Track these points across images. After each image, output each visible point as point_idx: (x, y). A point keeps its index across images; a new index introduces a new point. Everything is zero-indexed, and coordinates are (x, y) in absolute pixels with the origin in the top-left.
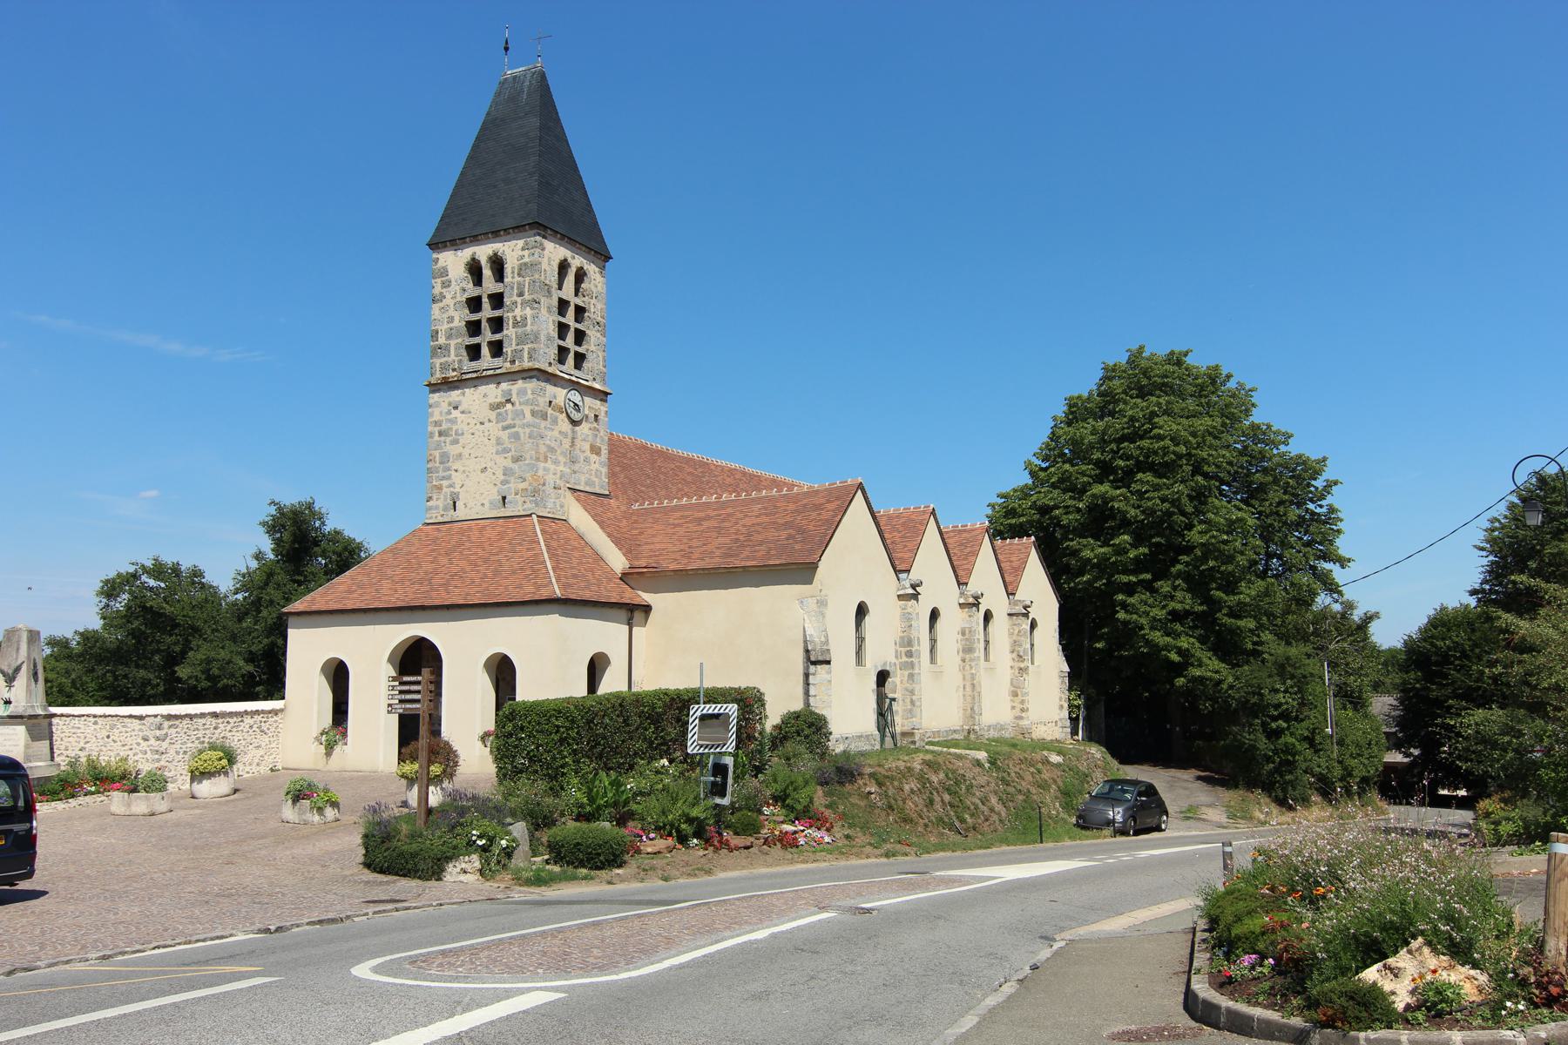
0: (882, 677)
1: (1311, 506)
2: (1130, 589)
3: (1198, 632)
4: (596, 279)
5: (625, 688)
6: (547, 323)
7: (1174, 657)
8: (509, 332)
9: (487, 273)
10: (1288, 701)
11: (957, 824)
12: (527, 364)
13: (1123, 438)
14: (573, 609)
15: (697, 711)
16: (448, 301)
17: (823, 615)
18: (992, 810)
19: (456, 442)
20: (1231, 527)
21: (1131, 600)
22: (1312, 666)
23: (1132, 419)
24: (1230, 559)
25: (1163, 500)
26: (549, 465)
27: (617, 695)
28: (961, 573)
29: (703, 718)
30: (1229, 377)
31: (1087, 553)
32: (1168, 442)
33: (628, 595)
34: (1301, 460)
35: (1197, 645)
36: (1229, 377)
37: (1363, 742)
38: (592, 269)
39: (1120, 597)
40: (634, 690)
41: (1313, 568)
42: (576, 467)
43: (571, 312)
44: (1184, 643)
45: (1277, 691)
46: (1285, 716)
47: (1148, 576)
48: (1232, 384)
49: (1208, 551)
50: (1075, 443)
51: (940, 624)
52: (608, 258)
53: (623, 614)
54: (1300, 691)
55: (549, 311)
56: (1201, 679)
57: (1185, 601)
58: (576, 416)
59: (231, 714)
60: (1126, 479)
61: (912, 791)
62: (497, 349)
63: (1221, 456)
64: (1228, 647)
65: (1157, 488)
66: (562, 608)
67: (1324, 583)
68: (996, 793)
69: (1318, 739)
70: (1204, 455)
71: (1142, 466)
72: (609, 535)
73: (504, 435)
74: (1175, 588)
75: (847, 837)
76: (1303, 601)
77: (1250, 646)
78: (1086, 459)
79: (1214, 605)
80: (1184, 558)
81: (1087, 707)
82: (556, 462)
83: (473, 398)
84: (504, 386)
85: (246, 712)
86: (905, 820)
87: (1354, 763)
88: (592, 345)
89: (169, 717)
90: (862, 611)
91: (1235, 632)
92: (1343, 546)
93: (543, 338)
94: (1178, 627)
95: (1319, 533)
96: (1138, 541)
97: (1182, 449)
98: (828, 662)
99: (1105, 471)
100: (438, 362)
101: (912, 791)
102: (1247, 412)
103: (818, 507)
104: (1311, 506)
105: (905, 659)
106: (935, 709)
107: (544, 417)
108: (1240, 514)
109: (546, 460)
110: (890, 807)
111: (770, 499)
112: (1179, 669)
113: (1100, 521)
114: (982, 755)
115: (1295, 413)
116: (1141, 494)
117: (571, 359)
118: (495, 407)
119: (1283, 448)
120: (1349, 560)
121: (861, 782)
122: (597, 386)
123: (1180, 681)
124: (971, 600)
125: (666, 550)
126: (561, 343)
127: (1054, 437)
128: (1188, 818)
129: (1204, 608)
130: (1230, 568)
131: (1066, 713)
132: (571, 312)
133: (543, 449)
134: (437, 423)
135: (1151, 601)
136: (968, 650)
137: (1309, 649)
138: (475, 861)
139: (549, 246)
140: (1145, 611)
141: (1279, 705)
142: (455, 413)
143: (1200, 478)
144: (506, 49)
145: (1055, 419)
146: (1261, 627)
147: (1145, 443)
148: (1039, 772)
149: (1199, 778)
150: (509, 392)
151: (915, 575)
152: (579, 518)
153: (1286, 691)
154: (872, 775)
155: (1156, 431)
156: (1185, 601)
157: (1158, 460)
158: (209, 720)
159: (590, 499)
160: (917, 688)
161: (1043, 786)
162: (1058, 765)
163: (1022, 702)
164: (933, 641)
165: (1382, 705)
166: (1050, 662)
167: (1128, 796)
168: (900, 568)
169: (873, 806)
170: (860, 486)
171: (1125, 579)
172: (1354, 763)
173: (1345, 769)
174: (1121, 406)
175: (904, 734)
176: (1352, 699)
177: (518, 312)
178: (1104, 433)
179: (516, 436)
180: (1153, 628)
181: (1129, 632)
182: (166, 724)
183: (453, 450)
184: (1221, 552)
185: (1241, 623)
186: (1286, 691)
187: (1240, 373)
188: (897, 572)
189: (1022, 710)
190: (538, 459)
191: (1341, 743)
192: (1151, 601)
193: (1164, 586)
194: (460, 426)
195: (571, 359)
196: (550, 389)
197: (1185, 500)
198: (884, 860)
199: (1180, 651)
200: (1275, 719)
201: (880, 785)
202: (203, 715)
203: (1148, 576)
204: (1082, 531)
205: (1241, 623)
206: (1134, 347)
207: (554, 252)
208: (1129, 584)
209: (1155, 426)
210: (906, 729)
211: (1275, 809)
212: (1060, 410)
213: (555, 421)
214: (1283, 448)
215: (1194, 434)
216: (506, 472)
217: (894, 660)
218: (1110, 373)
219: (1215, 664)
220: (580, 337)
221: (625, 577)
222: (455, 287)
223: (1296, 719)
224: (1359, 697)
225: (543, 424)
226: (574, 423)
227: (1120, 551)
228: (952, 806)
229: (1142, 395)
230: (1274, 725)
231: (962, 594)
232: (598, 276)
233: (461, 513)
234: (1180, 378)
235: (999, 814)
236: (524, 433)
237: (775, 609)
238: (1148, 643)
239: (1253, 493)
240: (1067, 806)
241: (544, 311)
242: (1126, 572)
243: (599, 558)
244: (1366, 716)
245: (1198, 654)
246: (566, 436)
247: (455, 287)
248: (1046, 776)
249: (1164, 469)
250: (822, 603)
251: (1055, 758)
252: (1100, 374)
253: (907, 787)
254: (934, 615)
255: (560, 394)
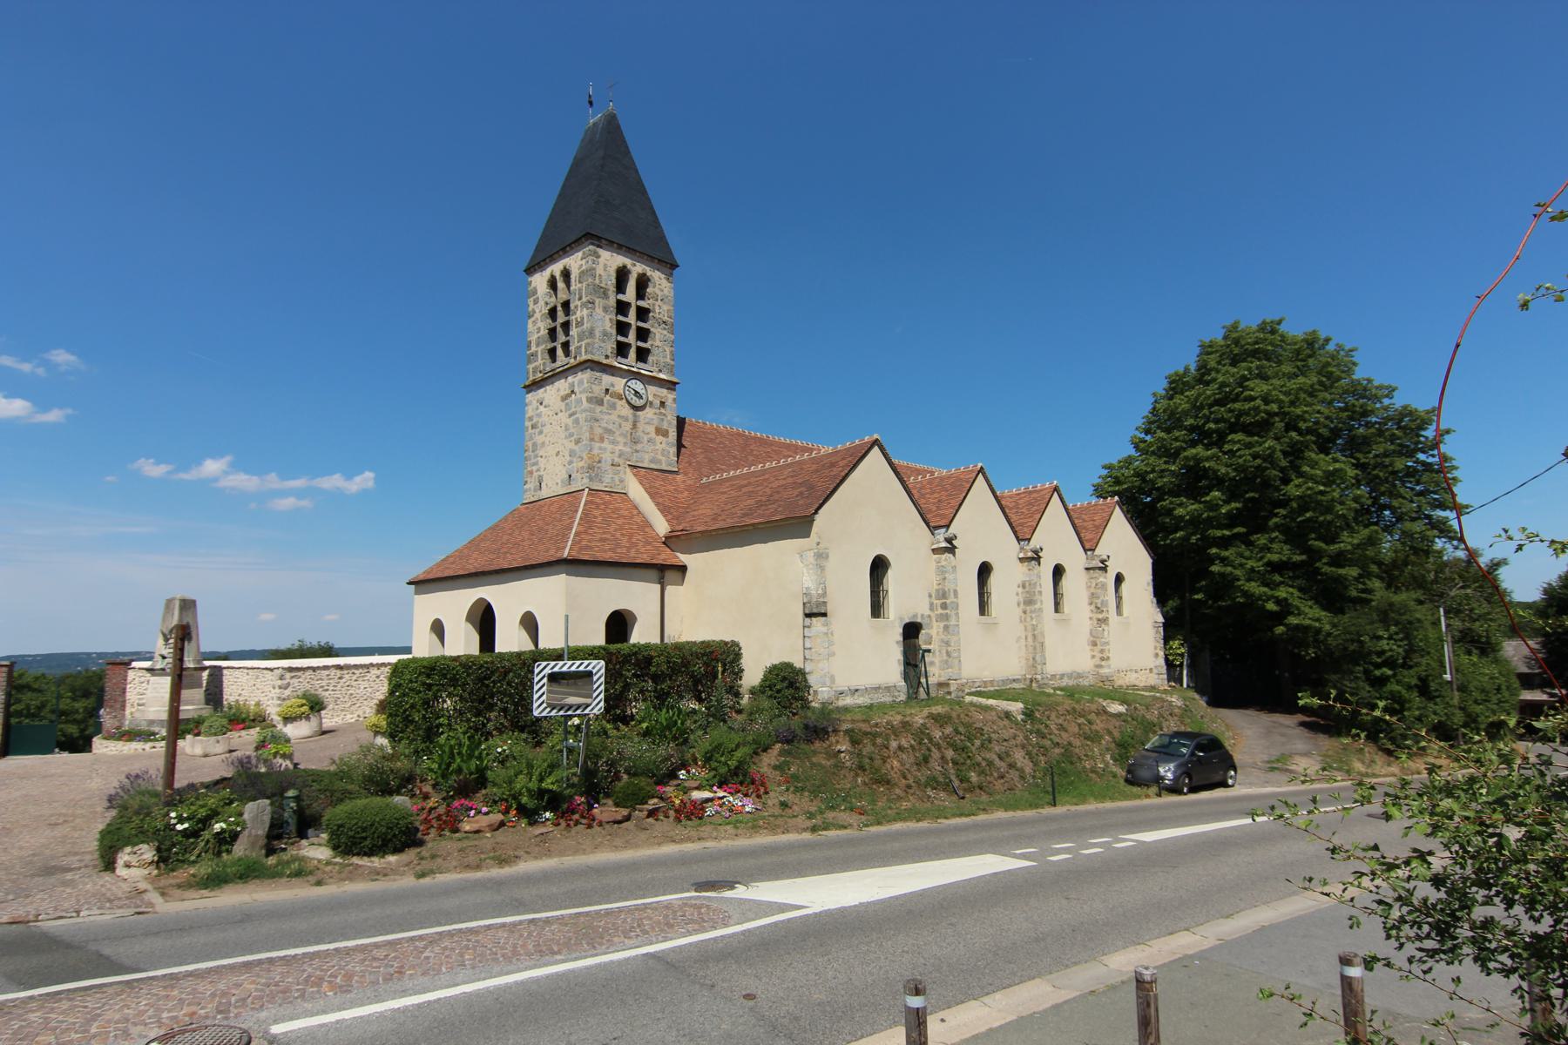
0: (911, 631)
1: (1421, 456)
2: (1224, 543)
3: (1298, 582)
4: (660, 283)
5: (658, 641)
6: (605, 322)
7: (1271, 606)
8: (574, 332)
9: (561, 285)
10: (1395, 649)
11: (956, 783)
12: (584, 357)
13: (1218, 403)
14: (582, 568)
15: (543, 669)
16: (538, 315)
17: (822, 568)
18: (1012, 766)
19: (541, 433)
20: (1331, 478)
21: (1225, 554)
22: (1421, 613)
23: (1223, 385)
24: (1329, 509)
25: (1255, 456)
26: (606, 444)
27: (647, 646)
28: (1086, 535)
29: (554, 678)
30: (1327, 340)
31: (1180, 511)
32: (1258, 401)
33: (665, 557)
34: (1407, 412)
35: (1296, 593)
36: (1327, 340)
37: (1488, 687)
38: (656, 276)
39: (1214, 551)
40: (571, 644)
41: (1428, 517)
42: (639, 447)
43: (633, 312)
44: (1282, 593)
45: (1380, 638)
46: (1389, 663)
47: (1241, 530)
48: (1331, 347)
49: (1305, 503)
50: (1172, 414)
51: (1124, 586)
52: (674, 266)
53: (654, 574)
54: (1407, 637)
55: (605, 309)
56: (1297, 627)
57: (1281, 552)
58: (639, 403)
59: (356, 667)
60: (1220, 440)
61: (900, 748)
62: (642, 355)
63: (1317, 412)
64: (1332, 597)
65: (1249, 446)
66: (570, 568)
67: (1441, 531)
68: (1023, 747)
69: (1433, 686)
70: (1298, 411)
71: (1234, 428)
72: (657, 504)
73: (570, 421)
74: (1272, 540)
75: (784, 805)
76: (1422, 550)
77: (1354, 593)
78: (1180, 427)
79: (1315, 555)
80: (1283, 512)
81: (1192, 656)
82: (613, 442)
83: (552, 393)
84: (570, 379)
85: (372, 665)
86: (878, 782)
87: (1478, 709)
88: (659, 339)
89: (291, 669)
90: (879, 567)
91: (1340, 580)
92: (1462, 494)
93: (597, 334)
94: (1277, 578)
95: (1437, 483)
96: (1232, 497)
97: (1274, 407)
98: (824, 615)
99: (1200, 435)
100: (531, 367)
101: (900, 748)
102: (1349, 372)
103: (833, 465)
104: (1421, 456)
105: (940, 611)
106: (982, 656)
107: (600, 402)
108: (1337, 465)
109: (602, 439)
110: (862, 768)
111: (800, 463)
112: (1279, 618)
113: (1194, 481)
114: (1016, 707)
115: (1395, 366)
116: (1231, 453)
117: (632, 354)
118: (564, 398)
119: (1386, 402)
120: (1467, 507)
121: (833, 739)
122: (662, 376)
123: (1280, 629)
124: (1030, 554)
125: (703, 516)
126: (620, 338)
127: (1154, 411)
128: (1272, 769)
129: (1304, 557)
130: (1329, 517)
131: (1161, 661)
132: (633, 312)
133: (598, 431)
134: (531, 419)
135: (1247, 553)
136: (1029, 602)
137: (1419, 594)
138: (148, 852)
139: (605, 255)
140: (1243, 566)
141: (1382, 653)
142: (541, 408)
143: (1294, 434)
144: (591, 103)
145: (1154, 394)
146: (1369, 575)
147: (1237, 405)
148: (1090, 722)
149: (1303, 724)
150: (572, 385)
151: (1035, 542)
152: (636, 492)
153: (1390, 638)
154: (847, 732)
155: (1247, 393)
156: (1281, 552)
157: (1249, 420)
158: (333, 671)
159: (651, 476)
160: (953, 639)
161: (1094, 738)
162: (1119, 715)
163: (1102, 651)
164: (1119, 599)
165: (1516, 652)
166: (1141, 614)
167: (1184, 750)
168: (1088, 547)
169: (839, 766)
170: (1056, 489)
171: (1218, 533)
172: (1478, 709)
173: (1468, 715)
174: (1213, 374)
175: (940, 685)
176: (1478, 644)
177: (579, 314)
178: (1196, 399)
179: (577, 421)
180: (1249, 580)
181: (1225, 585)
182: (288, 675)
183: (539, 439)
184: (1319, 503)
185: (1342, 571)
186: (1390, 638)
187: (1338, 332)
188: (1019, 540)
189: (1102, 659)
190: (592, 440)
191: (1462, 689)
192: (1247, 553)
193: (1262, 540)
194: (544, 419)
195: (632, 354)
196: (607, 379)
197: (1279, 454)
198: (807, 836)
199: (1278, 601)
200: (1378, 666)
201: (854, 742)
202: (326, 668)
203: (1241, 530)
204: (1175, 493)
205: (1342, 571)
206: (1228, 323)
207: (610, 261)
208: (1223, 538)
209: (1246, 388)
210: (942, 679)
211: (1380, 758)
212: (1161, 386)
213: (613, 407)
214: (1386, 402)
215: (1286, 394)
216: (572, 453)
217: (928, 612)
218: (1207, 349)
219: (1317, 612)
220: (643, 334)
221: (668, 541)
222: (541, 303)
223: (1404, 666)
224: (1488, 643)
225: (599, 409)
226: (636, 408)
227: (1213, 507)
228: (955, 763)
229: (1234, 363)
230: (1377, 673)
231: (1022, 549)
232: (665, 283)
233: (545, 493)
234: (1272, 344)
235: (1021, 770)
236: (581, 416)
237: (781, 560)
238: (1245, 594)
239: (1356, 446)
240: (1120, 759)
241: (599, 311)
242: (1220, 527)
243: (646, 524)
244: (1496, 661)
245: (1296, 602)
246: (626, 419)
247: (541, 303)
248: (1099, 725)
249: (1260, 428)
250: (821, 556)
251: (1116, 708)
252: (1198, 351)
253: (894, 744)
254: (985, 570)
255: (619, 383)
